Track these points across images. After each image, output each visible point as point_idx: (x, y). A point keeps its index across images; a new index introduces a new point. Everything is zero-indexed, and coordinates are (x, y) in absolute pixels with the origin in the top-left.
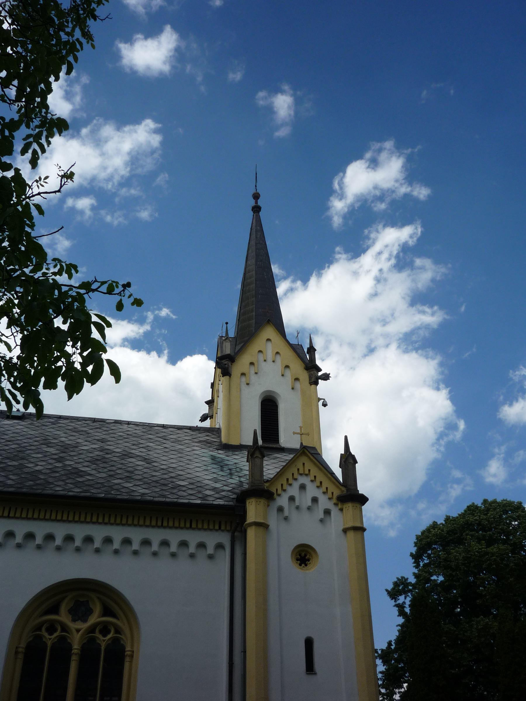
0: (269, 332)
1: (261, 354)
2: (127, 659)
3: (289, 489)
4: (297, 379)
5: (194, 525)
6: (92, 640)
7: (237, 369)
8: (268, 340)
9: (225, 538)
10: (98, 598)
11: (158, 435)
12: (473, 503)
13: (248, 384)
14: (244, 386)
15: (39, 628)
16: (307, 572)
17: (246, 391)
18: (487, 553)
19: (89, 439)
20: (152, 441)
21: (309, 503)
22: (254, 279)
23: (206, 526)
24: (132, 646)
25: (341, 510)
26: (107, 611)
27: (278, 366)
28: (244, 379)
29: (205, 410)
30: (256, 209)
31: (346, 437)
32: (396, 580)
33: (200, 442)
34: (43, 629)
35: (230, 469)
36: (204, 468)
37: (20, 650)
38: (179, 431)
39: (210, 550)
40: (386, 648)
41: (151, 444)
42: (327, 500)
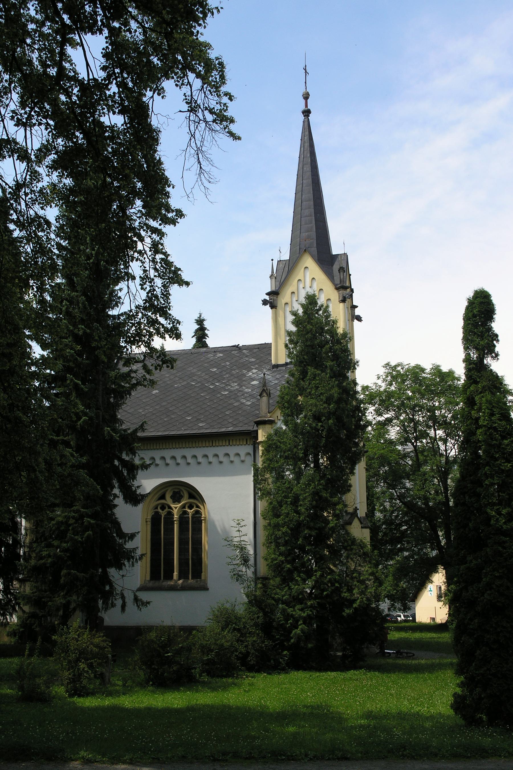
6: (185, 513)
10: (187, 490)
15: (156, 508)
26: (191, 496)
30: (307, 113)
34: (159, 508)
37: (148, 520)
40: (491, 370)
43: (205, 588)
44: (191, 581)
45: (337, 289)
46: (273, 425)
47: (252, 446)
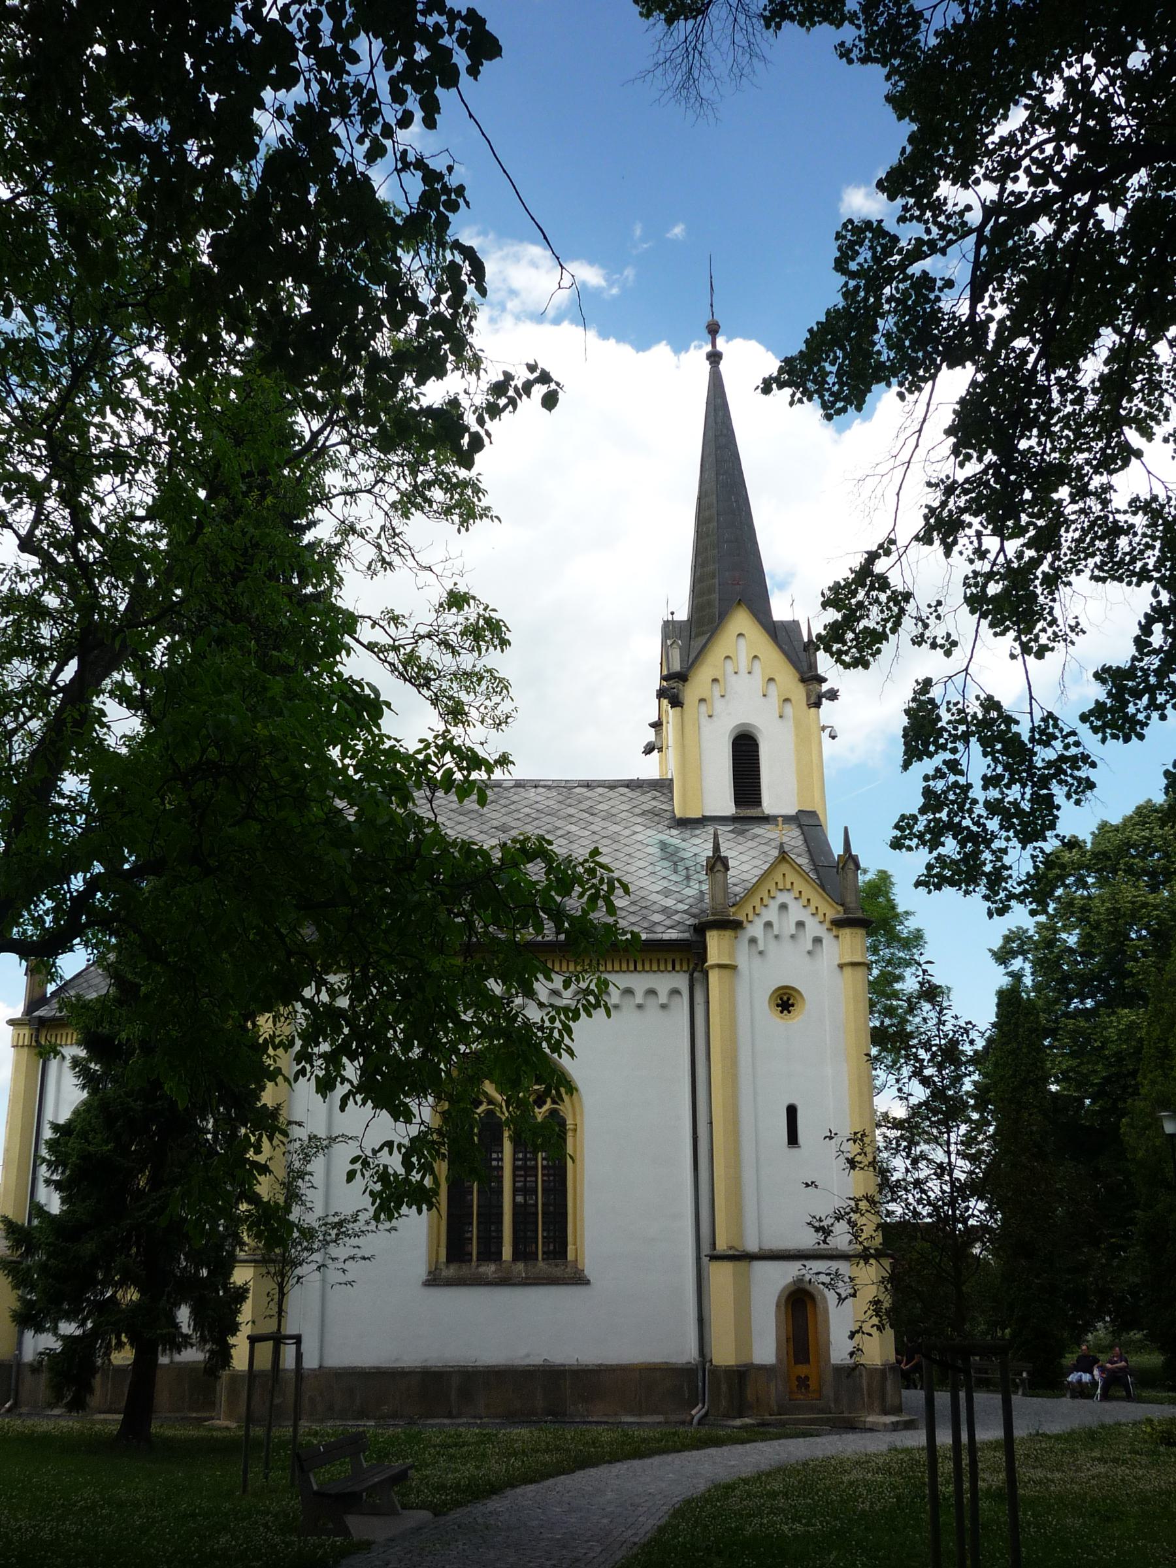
0: (741, 621)
1: (728, 662)
2: (570, 1134)
3: (764, 911)
4: (787, 700)
5: (639, 968)
7: (691, 693)
8: (740, 635)
9: (680, 981)
11: (582, 806)
12: (1150, 800)
13: (710, 716)
14: (704, 720)
16: (790, 1022)
17: (707, 727)
18: (1145, 905)
19: (485, 828)
20: (574, 820)
21: (792, 929)
22: (714, 511)
23: (655, 968)
24: (574, 1118)
25: (837, 937)
27: (758, 680)
28: (703, 708)
29: (651, 736)
31: (846, 829)
32: (1007, 933)
33: (643, 813)
35: (687, 868)
36: (650, 869)
38: (611, 794)
39: (663, 998)
41: (573, 828)
42: (819, 925)
43: (579, 1280)
44: (541, 1264)
45: (803, 680)
46: (740, 932)
47: (687, 976)
